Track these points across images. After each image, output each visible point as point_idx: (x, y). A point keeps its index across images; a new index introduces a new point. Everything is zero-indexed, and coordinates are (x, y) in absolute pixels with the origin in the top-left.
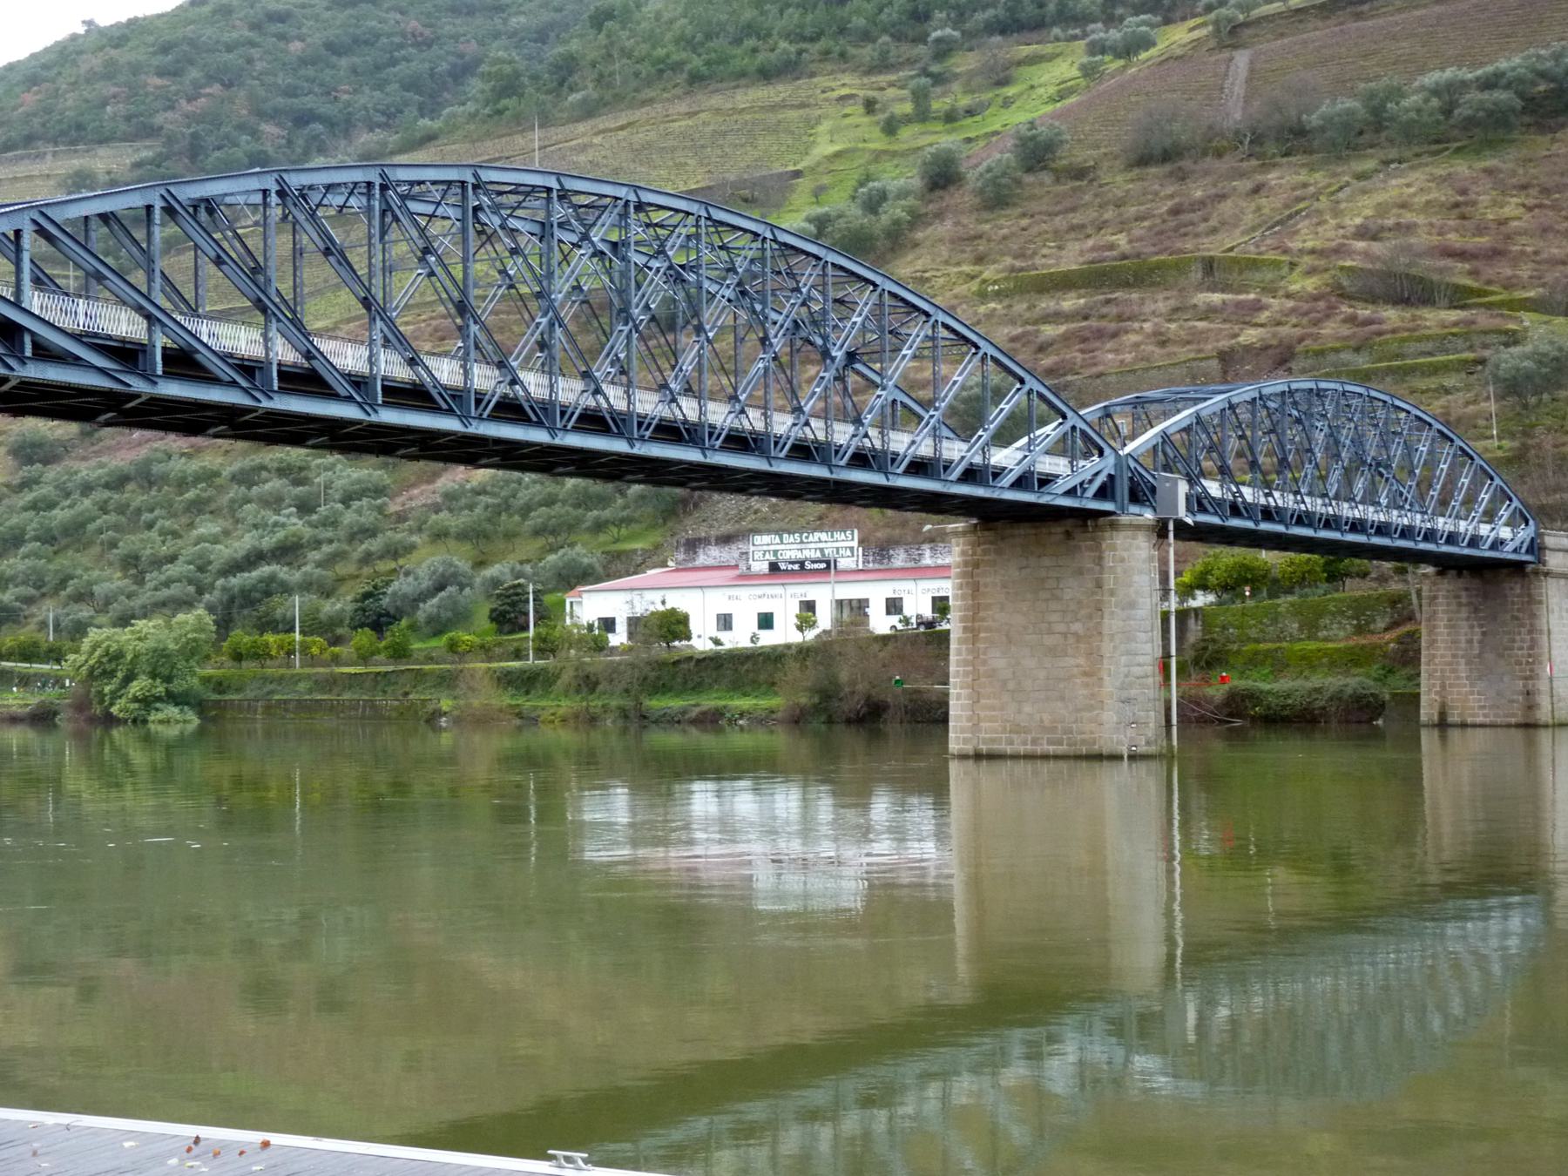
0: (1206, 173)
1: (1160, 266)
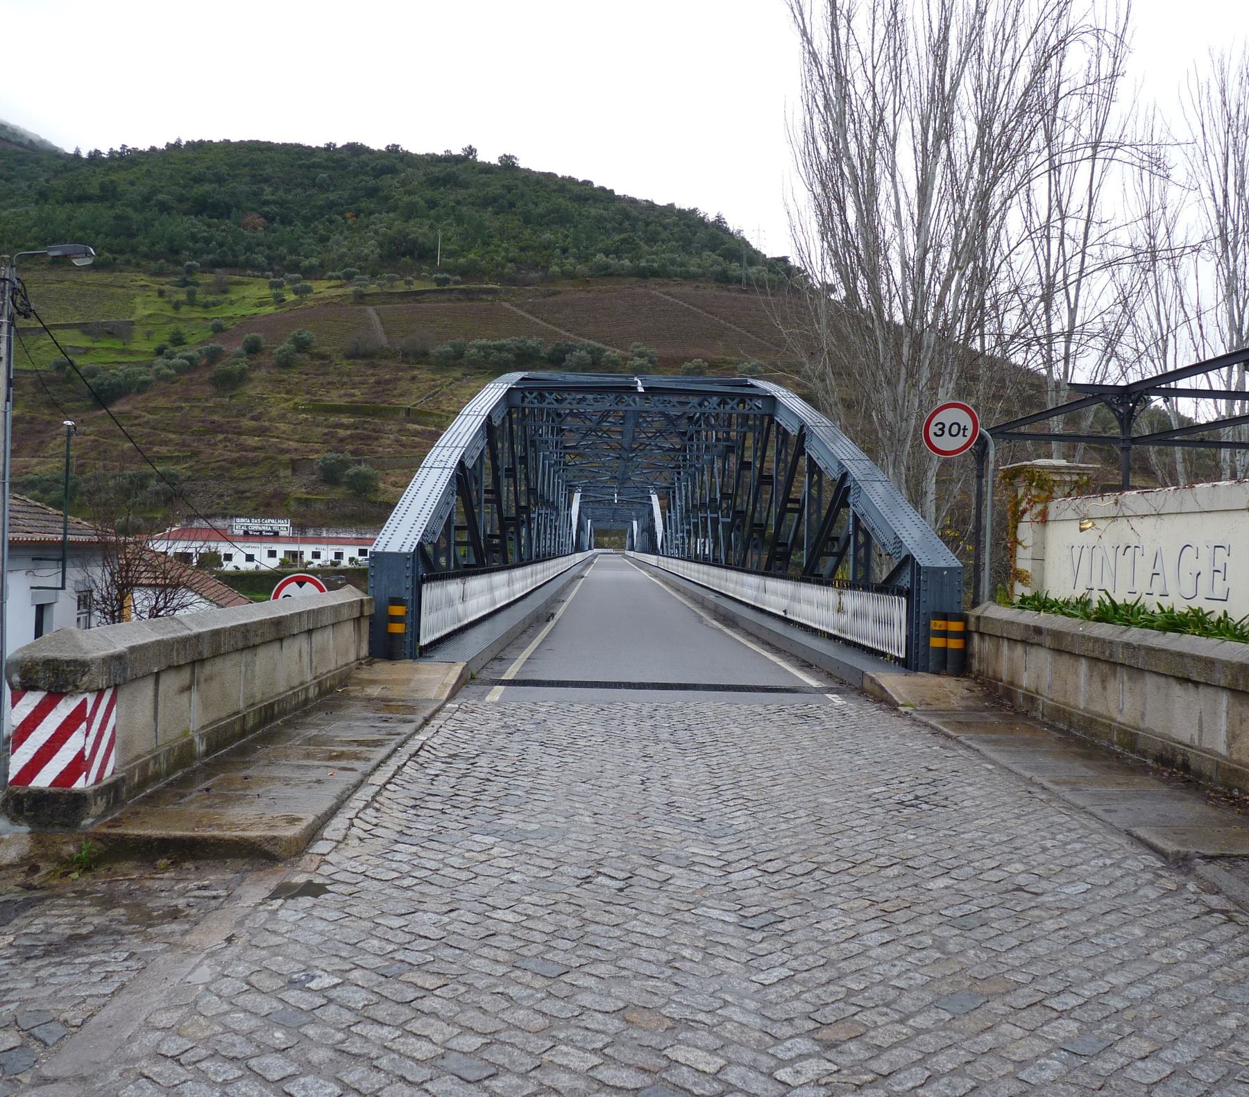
0: (386, 366)
1: (384, 409)
